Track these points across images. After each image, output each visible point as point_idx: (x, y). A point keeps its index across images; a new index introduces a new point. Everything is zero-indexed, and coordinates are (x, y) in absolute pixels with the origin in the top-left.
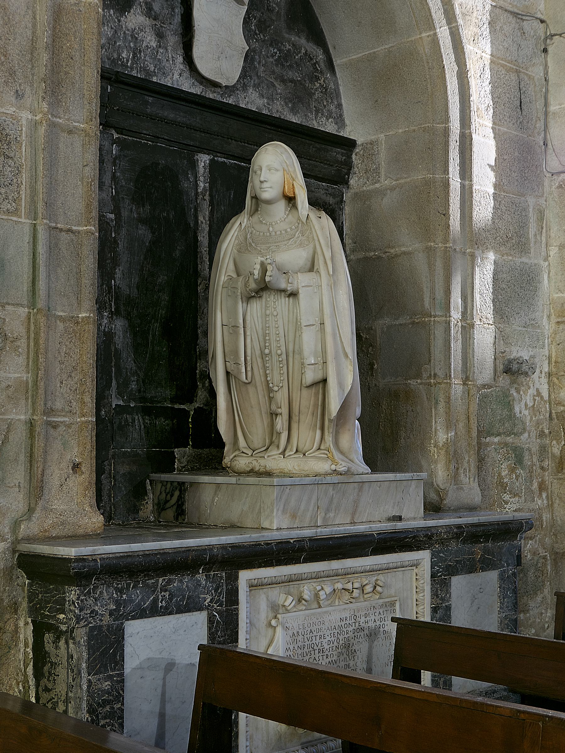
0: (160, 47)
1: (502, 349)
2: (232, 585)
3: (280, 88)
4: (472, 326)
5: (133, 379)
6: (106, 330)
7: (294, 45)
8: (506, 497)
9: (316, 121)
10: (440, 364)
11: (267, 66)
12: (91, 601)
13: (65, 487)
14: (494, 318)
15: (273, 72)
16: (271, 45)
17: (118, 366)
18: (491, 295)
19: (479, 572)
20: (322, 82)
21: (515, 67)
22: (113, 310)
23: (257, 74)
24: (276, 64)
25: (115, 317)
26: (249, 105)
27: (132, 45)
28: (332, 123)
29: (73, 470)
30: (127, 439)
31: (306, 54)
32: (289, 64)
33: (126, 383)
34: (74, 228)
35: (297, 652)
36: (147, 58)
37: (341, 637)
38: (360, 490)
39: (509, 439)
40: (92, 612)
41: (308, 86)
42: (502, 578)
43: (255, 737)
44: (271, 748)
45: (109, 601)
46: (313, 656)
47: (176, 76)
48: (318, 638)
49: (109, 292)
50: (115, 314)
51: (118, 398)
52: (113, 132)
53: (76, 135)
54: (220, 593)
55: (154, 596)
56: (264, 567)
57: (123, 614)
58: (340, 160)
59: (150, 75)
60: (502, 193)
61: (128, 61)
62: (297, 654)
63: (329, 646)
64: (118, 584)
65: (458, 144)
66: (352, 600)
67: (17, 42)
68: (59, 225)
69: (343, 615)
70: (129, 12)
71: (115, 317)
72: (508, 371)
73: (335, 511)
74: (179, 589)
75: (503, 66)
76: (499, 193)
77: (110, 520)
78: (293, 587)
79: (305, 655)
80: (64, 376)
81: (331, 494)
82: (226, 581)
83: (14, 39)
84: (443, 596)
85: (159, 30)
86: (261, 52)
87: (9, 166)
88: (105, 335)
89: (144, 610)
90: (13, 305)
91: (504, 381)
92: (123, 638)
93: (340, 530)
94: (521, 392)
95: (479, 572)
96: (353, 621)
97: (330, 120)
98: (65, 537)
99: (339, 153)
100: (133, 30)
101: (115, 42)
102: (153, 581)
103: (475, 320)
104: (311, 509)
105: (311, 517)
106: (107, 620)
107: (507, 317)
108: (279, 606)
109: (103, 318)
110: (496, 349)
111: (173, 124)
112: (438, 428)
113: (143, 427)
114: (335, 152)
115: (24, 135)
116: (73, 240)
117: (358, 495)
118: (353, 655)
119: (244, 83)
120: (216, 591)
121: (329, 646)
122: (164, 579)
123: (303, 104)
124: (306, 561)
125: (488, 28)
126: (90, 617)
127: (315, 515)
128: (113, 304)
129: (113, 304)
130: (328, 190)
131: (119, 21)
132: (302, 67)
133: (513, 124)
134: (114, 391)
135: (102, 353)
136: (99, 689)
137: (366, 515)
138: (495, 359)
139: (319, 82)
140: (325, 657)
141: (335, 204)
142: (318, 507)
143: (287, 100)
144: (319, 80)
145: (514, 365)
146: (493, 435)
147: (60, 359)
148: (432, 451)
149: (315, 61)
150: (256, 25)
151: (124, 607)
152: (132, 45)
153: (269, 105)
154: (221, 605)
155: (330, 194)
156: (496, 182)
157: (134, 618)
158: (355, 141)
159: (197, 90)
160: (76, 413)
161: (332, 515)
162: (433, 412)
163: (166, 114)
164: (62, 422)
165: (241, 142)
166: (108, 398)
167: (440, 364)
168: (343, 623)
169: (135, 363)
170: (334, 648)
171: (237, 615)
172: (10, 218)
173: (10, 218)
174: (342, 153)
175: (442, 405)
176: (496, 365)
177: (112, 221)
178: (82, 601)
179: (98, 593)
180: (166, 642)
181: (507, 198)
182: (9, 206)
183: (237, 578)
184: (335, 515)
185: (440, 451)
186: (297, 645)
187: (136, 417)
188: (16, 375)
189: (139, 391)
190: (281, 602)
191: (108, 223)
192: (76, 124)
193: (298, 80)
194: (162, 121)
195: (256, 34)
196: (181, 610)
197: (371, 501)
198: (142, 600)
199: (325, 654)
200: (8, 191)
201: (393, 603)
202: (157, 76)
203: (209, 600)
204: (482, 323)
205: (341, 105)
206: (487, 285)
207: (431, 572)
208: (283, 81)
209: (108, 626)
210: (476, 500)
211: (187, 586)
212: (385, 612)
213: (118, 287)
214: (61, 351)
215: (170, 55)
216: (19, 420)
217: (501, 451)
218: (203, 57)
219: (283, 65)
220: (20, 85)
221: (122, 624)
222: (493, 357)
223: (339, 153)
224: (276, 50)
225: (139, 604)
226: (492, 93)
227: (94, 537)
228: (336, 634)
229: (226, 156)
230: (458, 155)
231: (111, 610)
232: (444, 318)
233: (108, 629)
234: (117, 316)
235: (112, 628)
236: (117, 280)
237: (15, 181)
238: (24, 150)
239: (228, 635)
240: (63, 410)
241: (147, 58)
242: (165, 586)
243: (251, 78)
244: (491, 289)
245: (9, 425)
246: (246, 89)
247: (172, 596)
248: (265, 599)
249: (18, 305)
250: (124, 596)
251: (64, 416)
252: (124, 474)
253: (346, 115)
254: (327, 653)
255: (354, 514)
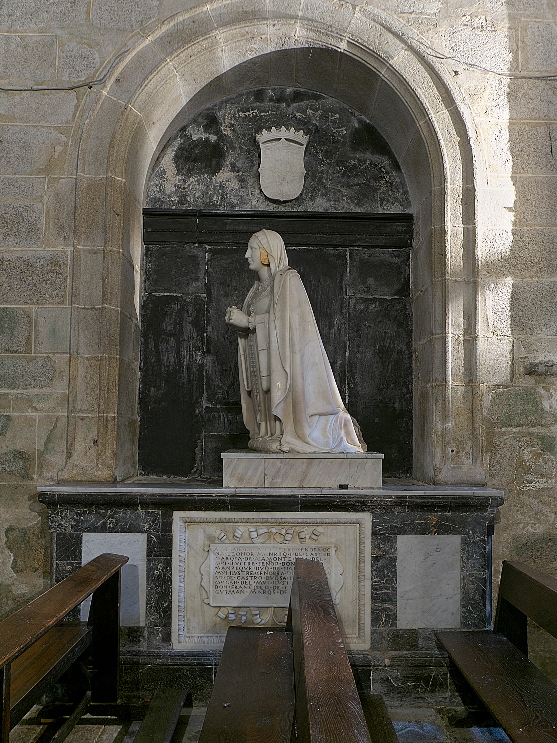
0: (242, 188)
1: (523, 354)
2: (167, 520)
3: (345, 191)
4: (475, 339)
5: (219, 391)
6: (200, 363)
7: (358, 160)
8: (529, 477)
9: (382, 208)
10: (439, 371)
11: (334, 180)
12: (59, 518)
13: (88, 453)
14: (512, 330)
15: (340, 182)
16: (337, 165)
17: (208, 385)
18: (508, 312)
19: (435, 535)
20: (387, 179)
21: (543, 121)
22: (205, 351)
23: (324, 187)
24: (341, 177)
25: (206, 355)
26: (316, 208)
27: (220, 191)
28: (398, 206)
29: (94, 444)
30: (214, 427)
31: (371, 163)
32: (355, 174)
33: (215, 394)
34: (96, 307)
35: (226, 570)
36: (232, 197)
37: (270, 566)
38: (310, 464)
39: (535, 430)
40: (59, 524)
41: (373, 185)
42: (464, 542)
43: (192, 620)
44: (207, 630)
45: (71, 520)
46: (241, 575)
47: (254, 203)
48: (246, 564)
49: (202, 341)
50: (206, 353)
51: (207, 403)
52: (206, 245)
53: (99, 254)
54: (157, 524)
55: (104, 520)
56: (194, 511)
57: (81, 528)
58: (401, 230)
59: (234, 206)
60: (525, 228)
61: (217, 202)
62: (226, 572)
63: (258, 571)
64: (78, 511)
65: (461, 197)
66: (285, 542)
67: (65, 210)
68: (86, 307)
69: (273, 551)
70: (219, 172)
71: (206, 355)
72: (531, 373)
73: (283, 478)
74: (123, 518)
75: (527, 124)
76: (520, 228)
77: (202, 475)
78: (229, 527)
79: (234, 573)
80: (89, 391)
81: (279, 466)
82: (162, 516)
83: (64, 209)
84: (387, 549)
85: (241, 178)
86: (328, 171)
87: (60, 278)
88: (199, 366)
89: (97, 528)
90: (61, 353)
91: (528, 382)
92: (81, 543)
93: (245, 491)
94: (551, 390)
95: (435, 535)
96: (283, 556)
97: (395, 204)
98: (87, 481)
99: (399, 226)
100: (221, 183)
101: (208, 193)
102: (103, 511)
103: (477, 334)
104: (258, 475)
105: (258, 481)
106: (69, 530)
107: (530, 328)
108: (215, 538)
109: (197, 356)
110: (513, 356)
111: (248, 233)
112: (438, 420)
113: (226, 420)
114: (395, 226)
115: (69, 260)
116: (96, 313)
117: (307, 468)
118: (282, 581)
119: (312, 195)
120: (153, 522)
121: (258, 571)
122: (112, 511)
123: (368, 198)
124: (232, 510)
125: (506, 98)
126: (58, 527)
127: (263, 479)
128: (205, 347)
129: (205, 347)
130: (393, 254)
131: (211, 180)
132: (367, 174)
133: (541, 168)
134: (205, 398)
135: (197, 376)
136: (63, 569)
137: (316, 482)
138: (513, 364)
139: (384, 180)
140: (253, 578)
141: (401, 262)
142: (265, 475)
143: (352, 199)
144: (385, 178)
145: (539, 368)
146: (511, 426)
147: (86, 381)
148: (433, 438)
149: (380, 166)
150: (323, 155)
151: (82, 524)
152: (220, 191)
153: (336, 205)
154: (157, 531)
155: (396, 256)
156: (516, 220)
157: (88, 531)
158: (412, 214)
159: (271, 208)
160: (97, 411)
161: (279, 480)
162: (434, 408)
163: (241, 227)
164: (87, 417)
165: (306, 234)
166: (200, 403)
167: (439, 371)
168: (272, 557)
169: (221, 381)
170: (263, 573)
171: (171, 539)
172: (59, 306)
173: (59, 306)
174: (403, 225)
175: (440, 404)
176: (513, 369)
177: (205, 298)
178: (53, 517)
179: (64, 514)
180: (114, 549)
181: (532, 230)
182: (59, 300)
183: (171, 516)
184: (282, 481)
185: (439, 438)
186: (226, 566)
187: (222, 414)
188: (62, 391)
189: (224, 398)
190: (217, 536)
191: (202, 300)
192: (99, 248)
193: (362, 183)
194: (239, 233)
195: (323, 161)
196: (130, 531)
197: (321, 473)
198: (95, 521)
199: (254, 576)
200: (59, 292)
201: (327, 548)
202: (239, 206)
203: (147, 527)
204: (495, 336)
205: (407, 191)
206: (503, 304)
207: (372, 530)
208: (349, 186)
209: (70, 534)
210: (477, 478)
211: (130, 517)
212: (318, 555)
213: (208, 337)
214: (87, 376)
215: (250, 191)
216: (64, 415)
217: (522, 439)
218: (268, 186)
219: (349, 176)
220: (67, 233)
221: (80, 534)
222: (510, 363)
223: (399, 226)
224: (341, 168)
225: (93, 523)
226: (511, 150)
227: (107, 483)
228: (265, 564)
229: (295, 245)
230: (461, 206)
231: (72, 525)
232: (442, 335)
233: (70, 536)
234: (208, 354)
235: (73, 535)
236: (208, 333)
237: (63, 285)
238: (68, 268)
239: (163, 551)
240: (88, 410)
241: (232, 197)
242: (112, 515)
243: (319, 191)
244: (508, 308)
245: (57, 418)
246: (314, 199)
247: (117, 522)
248: (202, 532)
249: (63, 353)
250: (82, 518)
251: (88, 413)
252: (212, 448)
253: (411, 199)
254: (255, 575)
255: (302, 480)
